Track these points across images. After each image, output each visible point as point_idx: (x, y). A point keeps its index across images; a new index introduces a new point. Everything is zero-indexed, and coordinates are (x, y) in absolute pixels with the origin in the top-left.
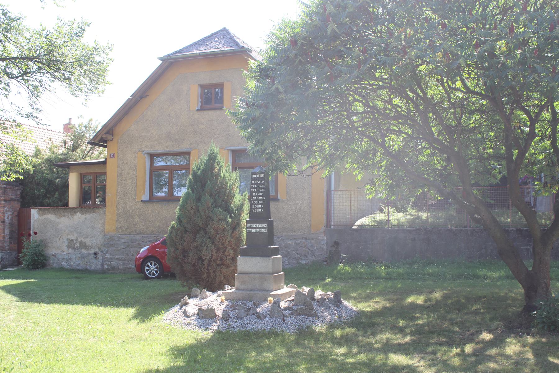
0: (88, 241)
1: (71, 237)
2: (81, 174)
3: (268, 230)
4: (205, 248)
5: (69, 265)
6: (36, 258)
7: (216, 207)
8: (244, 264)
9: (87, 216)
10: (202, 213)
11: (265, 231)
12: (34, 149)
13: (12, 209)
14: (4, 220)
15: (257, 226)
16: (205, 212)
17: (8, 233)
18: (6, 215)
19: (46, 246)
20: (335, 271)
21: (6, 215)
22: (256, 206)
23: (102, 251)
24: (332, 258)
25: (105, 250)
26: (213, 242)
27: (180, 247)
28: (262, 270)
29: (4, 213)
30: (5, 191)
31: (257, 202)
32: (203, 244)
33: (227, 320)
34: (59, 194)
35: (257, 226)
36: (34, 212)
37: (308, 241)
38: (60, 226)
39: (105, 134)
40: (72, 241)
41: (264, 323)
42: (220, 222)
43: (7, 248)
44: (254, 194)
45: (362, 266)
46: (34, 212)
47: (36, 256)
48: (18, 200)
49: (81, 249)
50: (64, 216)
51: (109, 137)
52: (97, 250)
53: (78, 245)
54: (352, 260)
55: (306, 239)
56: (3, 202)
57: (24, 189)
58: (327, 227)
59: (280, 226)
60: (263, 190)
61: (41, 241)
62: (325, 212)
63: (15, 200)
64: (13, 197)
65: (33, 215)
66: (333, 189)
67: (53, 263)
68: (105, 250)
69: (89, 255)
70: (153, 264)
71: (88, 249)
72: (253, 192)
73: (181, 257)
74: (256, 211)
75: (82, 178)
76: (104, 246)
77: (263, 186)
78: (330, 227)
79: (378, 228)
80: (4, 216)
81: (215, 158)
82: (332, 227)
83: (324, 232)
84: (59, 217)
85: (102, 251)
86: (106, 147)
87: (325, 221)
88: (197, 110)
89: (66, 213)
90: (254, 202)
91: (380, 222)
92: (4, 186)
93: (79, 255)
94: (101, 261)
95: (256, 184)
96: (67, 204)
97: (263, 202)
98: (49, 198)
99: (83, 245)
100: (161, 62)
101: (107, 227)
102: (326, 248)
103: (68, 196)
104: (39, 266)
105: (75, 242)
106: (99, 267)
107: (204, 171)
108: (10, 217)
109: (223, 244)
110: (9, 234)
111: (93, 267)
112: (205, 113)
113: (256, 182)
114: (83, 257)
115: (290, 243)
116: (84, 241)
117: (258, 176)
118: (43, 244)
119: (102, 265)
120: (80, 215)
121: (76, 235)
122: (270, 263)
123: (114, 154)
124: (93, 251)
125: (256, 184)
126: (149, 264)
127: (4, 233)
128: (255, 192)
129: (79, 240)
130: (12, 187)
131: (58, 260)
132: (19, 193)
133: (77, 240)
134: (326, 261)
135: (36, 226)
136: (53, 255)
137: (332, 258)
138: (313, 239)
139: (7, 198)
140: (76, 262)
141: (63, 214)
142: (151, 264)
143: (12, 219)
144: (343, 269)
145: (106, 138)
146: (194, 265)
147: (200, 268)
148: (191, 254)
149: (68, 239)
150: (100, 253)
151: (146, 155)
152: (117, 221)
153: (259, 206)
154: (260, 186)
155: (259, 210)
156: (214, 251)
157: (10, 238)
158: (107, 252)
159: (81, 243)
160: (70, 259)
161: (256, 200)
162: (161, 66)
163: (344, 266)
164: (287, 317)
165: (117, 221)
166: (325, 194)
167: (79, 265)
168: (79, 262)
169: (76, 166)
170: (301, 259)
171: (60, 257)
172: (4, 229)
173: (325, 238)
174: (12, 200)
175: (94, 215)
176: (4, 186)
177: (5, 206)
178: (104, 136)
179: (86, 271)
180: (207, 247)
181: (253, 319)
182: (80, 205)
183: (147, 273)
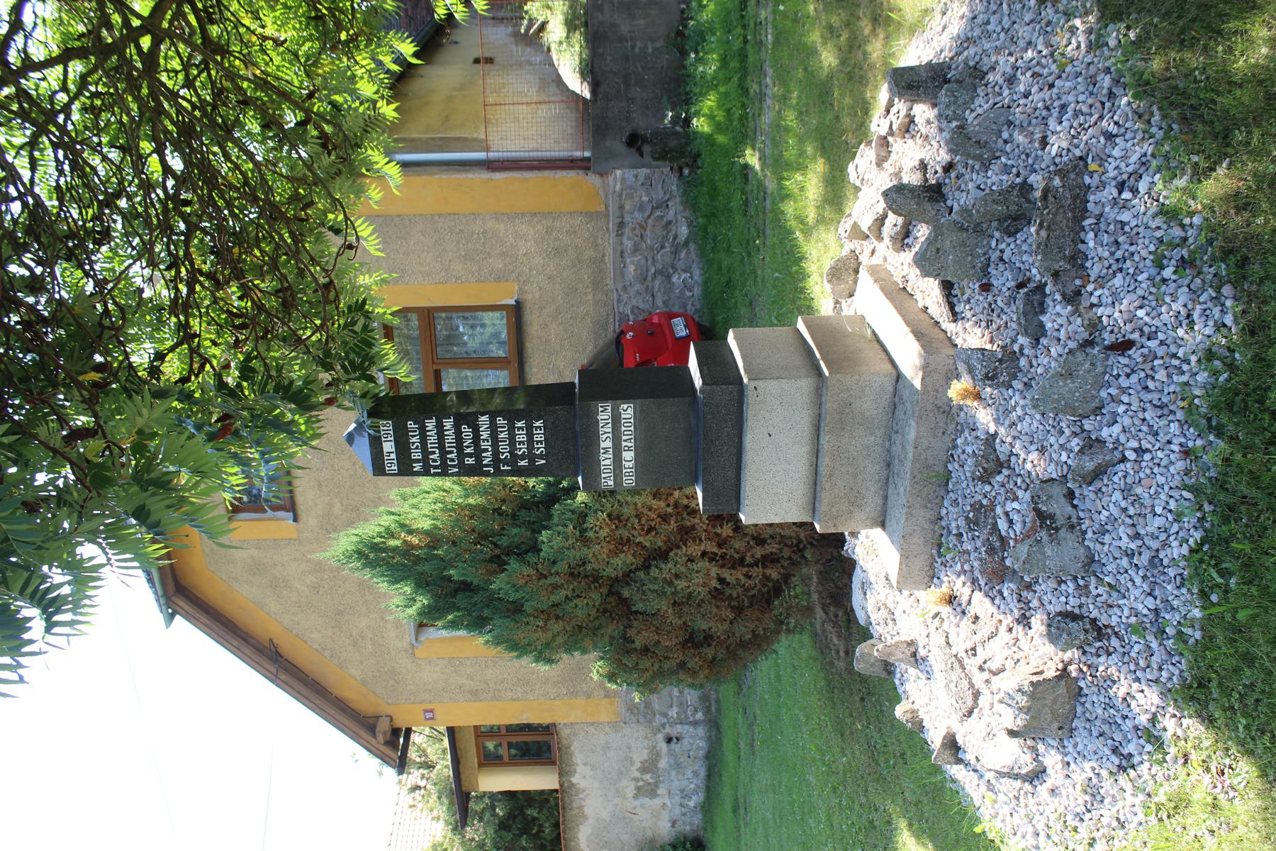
0: (640, 755)
1: (630, 791)
2: (481, 765)
3: (626, 398)
4: (681, 584)
5: (696, 792)
7: (535, 549)
8: (772, 495)
9: (579, 762)
10: (559, 596)
11: (628, 411)
15: (606, 444)
16: (556, 587)
19: (652, 841)
20: (721, 139)
22: (522, 449)
23: (663, 726)
24: (679, 151)
25: (659, 720)
26: (662, 555)
27: (678, 656)
28: (803, 419)
31: (504, 448)
32: (669, 590)
33: (1099, 631)
34: (530, 806)
35: (606, 444)
37: (627, 218)
38: (605, 815)
39: (374, 736)
40: (638, 789)
41: (1140, 451)
42: (590, 534)
44: (471, 461)
45: (699, 60)
49: (658, 769)
51: (384, 726)
52: (660, 737)
53: (648, 777)
54: (680, 91)
55: (621, 225)
58: (588, 168)
59: (590, 297)
60: (448, 424)
62: (546, 173)
66: (481, 155)
67: (691, 824)
68: (659, 720)
69: (671, 754)
71: (658, 755)
72: (461, 465)
73: (709, 652)
74: (540, 449)
75: (490, 761)
76: (650, 721)
77: (431, 424)
78: (588, 159)
79: (586, 24)
81: (375, 547)
82: (587, 154)
83: (601, 175)
84: (585, 817)
85: (663, 726)
86: (409, 731)
87: (571, 175)
88: (295, 520)
89: (575, 805)
90: (506, 462)
91: (571, 25)
93: (673, 773)
94: (686, 727)
95: (426, 453)
97: (500, 421)
98: (540, 831)
99: (649, 766)
100: (178, 617)
101: (604, 718)
102: (644, 171)
105: (641, 783)
106: (701, 731)
107: (422, 584)
109: (664, 518)
111: (702, 744)
112: (300, 500)
113: (416, 455)
114: (678, 766)
115: (632, 268)
116: (638, 765)
117: (388, 446)
119: (695, 724)
121: (625, 782)
122: (771, 387)
123: (426, 711)
124: (663, 746)
125: (426, 453)
128: (461, 454)
129: (637, 774)
131: (684, 814)
133: (636, 780)
134: (681, 169)
136: (673, 826)
137: (679, 151)
138: (621, 207)
140: (691, 779)
141: (576, 812)
144: (711, 117)
145: (385, 733)
146: (738, 610)
147: (747, 590)
148: (702, 624)
149: (636, 797)
150: (668, 729)
151: (422, 638)
152: (589, 697)
153: (521, 436)
154: (432, 438)
155: (539, 436)
156: (694, 549)
158: (665, 715)
159: (644, 770)
160: (682, 791)
161: (496, 453)
162: (188, 617)
163: (697, 114)
164: (1095, 326)
165: (589, 697)
166: (498, 176)
167: (695, 773)
168: (689, 773)
169: (463, 777)
170: (675, 237)
171: (677, 811)
173: (618, 172)
175: (575, 747)
178: (381, 738)
179: (713, 759)
180: (677, 576)
181: (1106, 503)
182: (554, 763)
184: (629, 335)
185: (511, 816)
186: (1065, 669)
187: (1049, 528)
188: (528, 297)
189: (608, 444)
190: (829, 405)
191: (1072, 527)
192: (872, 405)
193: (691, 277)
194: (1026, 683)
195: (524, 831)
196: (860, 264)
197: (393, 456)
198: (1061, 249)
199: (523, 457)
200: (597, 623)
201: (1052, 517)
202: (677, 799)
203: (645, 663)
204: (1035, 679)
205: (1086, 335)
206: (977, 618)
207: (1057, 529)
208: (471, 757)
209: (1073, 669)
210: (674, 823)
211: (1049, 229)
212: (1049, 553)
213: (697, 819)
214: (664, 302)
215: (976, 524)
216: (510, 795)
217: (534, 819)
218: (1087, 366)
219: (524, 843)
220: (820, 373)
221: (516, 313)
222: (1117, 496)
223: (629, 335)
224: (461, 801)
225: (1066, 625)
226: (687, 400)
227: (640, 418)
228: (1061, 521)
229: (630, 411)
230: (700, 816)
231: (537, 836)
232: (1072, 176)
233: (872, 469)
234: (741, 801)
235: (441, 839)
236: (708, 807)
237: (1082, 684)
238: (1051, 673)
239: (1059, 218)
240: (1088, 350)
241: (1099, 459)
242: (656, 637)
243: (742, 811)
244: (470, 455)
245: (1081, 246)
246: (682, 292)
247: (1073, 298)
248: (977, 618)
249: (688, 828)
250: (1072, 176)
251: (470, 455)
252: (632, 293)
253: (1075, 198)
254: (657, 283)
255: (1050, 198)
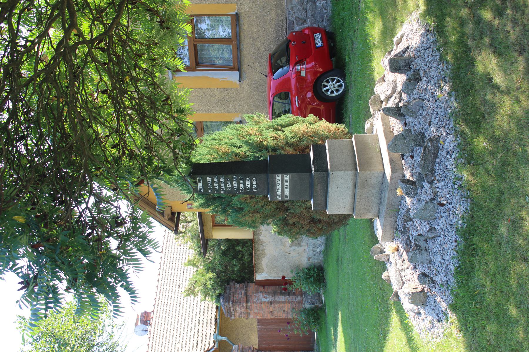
5: (320, 245)
6: (312, 279)
11: (287, 177)
12: (189, 267)
13: (256, 293)
14: (268, 302)
17: (283, 297)
18: (263, 300)
19: (298, 266)
21: (263, 300)
29: (261, 303)
30: (236, 303)
35: (279, 186)
36: (259, 277)
39: (163, 216)
43: (299, 298)
44: (230, 189)
46: (259, 277)
47: (309, 278)
48: (247, 287)
50: (263, 250)
51: (168, 212)
56: (249, 304)
57: (233, 280)
59: (274, 12)
60: (222, 178)
61: (292, 272)
63: (246, 290)
64: (243, 292)
65: (262, 277)
67: (318, 259)
70: (325, 84)
73: (320, 226)
74: (255, 186)
77: (215, 178)
80: (264, 302)
84: (265, 254)
86: (179, 213)
89: (260, 249)
90: (242, 190)
92: (231, 303)
96: (251, 240)
103: (243, 239)
104: (321, 275)
108: (265, 296)
110: (285, 296)
113: (210, 187)
118: (297, 269)
120: (262, 235)
126: (325, 89)
127: (283, 302)
130: (232, 294)
132: (238, 286)
135: (276, 275)
136: (309, 260)
139: (245, 300)
142: (325, 86)
143: (268, 293)
145: (168, 215)
149: (291, 246)
153: (248, 182)
154: (216, 182)
155: (254, 182)
157: (289, 295)
169: (205, 232)
171: (311, 253)
172: (279, 302)
174: (246, 294)
176: (231, 303)
177: (254, 302)
178: (166, 217)
181: (435, 247)
183: (336, 94)
184: (293, 43)
185: (228, 249)
186: (423, 289)
187: (419, 250)
188: (242, 11)
189: (280, 187)
190: (359, 180)
191: (426, 250)
192: (375, 181)
193: (327, 3)
194: (411, 292)
195: (234, 257)
196: (401, 42)
197: (201, 187)
198: (428, 168)
199: (248, 189)
200: (274, 213)
201: (420, 246)
202: (311, 248)
203: (294, 230)
204: (414, 291)
205: (432, 197)
206: (404, 260)
207: (421, 250)
208: (209, 223)
209: (426, 289)
210: (309, 259)
211: (425, 160)
212: (418, 257)
213: (321, 257)
214: (312, 15)
215: (404, 233)
216: (228, 240)
217: (240, 251)
218: (432, 206)
219: (234, 263)
220: (356, 170)
221: (236, 19)
222: (438, 246)
223: (293, 43)
224: (204, 244)
225: (423, 277)
226: (308, 174)
227: (291, 180)
228: (423, 248)
229: (288, 177)
230: (322, 256)
231: (241, 259)
232: (435, 142)
233: (375, 200)
234: (340, 259)
235: (193, 259)
236: (326, 252)
237: (428, 294)
238: (419, 290)
239: (429, 157)
240: (433, 201)
241: (433, 235)
242: (298, 220)
243: (340, 262)
244: (229, 188)
245: (434, 167)
246: (321, 10)
247: (431, 182)
248: (404, 260)
249: (316, 261)
250: (435, 142)
251: (229, 188)
252: (296, 10)
253: (435, 150)
254: (309, 5)
255: (427, 150)
